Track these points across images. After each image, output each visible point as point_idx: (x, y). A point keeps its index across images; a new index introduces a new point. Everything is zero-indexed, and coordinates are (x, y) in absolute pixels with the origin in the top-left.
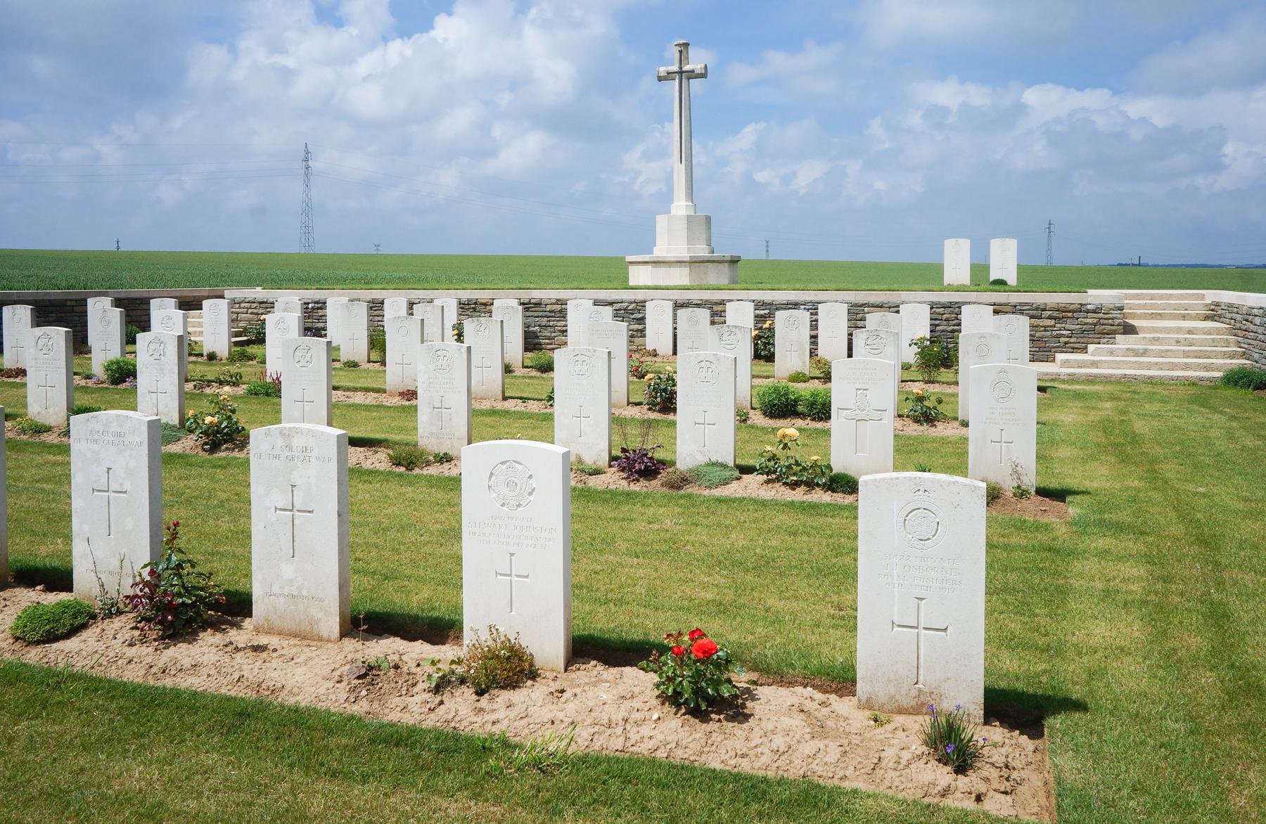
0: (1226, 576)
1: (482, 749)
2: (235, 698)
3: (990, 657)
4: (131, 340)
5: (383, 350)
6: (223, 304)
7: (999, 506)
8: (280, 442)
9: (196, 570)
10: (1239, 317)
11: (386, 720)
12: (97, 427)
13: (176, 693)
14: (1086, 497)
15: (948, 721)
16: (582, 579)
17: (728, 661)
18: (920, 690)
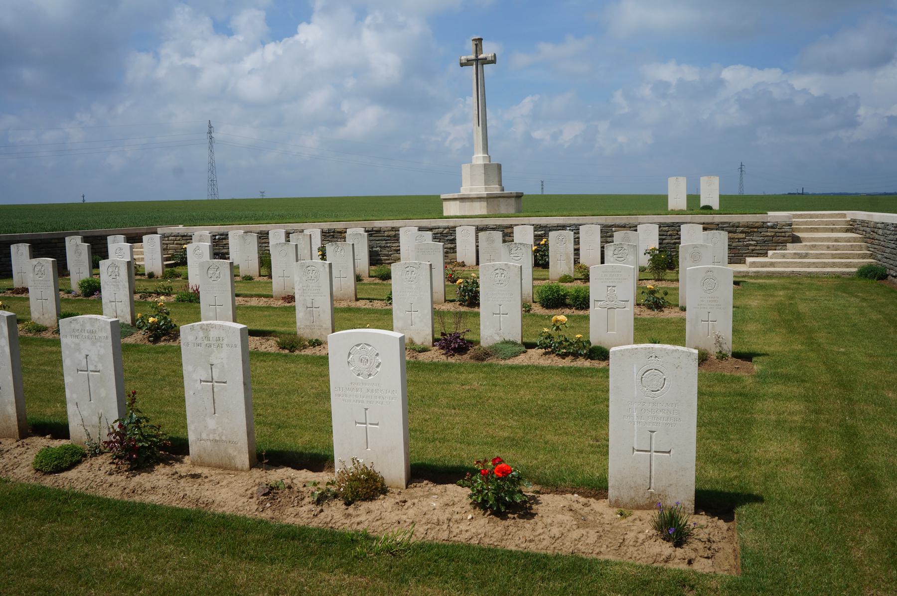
0: (856, 408)
1: (350, 541)
2: (182, 509)
3: (699, 469)
4: (95, 265)
5: (270, 267)
6: (157, 238)
7: (706, 366)
8: (201, 334)
9: (149, 424)
10: (868, 230)
11: (284, 522)
12: (78, 327)
13: (143, 506)
14: (765, 358)
15: (670, 513)
16: (416, 425)
17: (519, 478)
18: (651, 493)
